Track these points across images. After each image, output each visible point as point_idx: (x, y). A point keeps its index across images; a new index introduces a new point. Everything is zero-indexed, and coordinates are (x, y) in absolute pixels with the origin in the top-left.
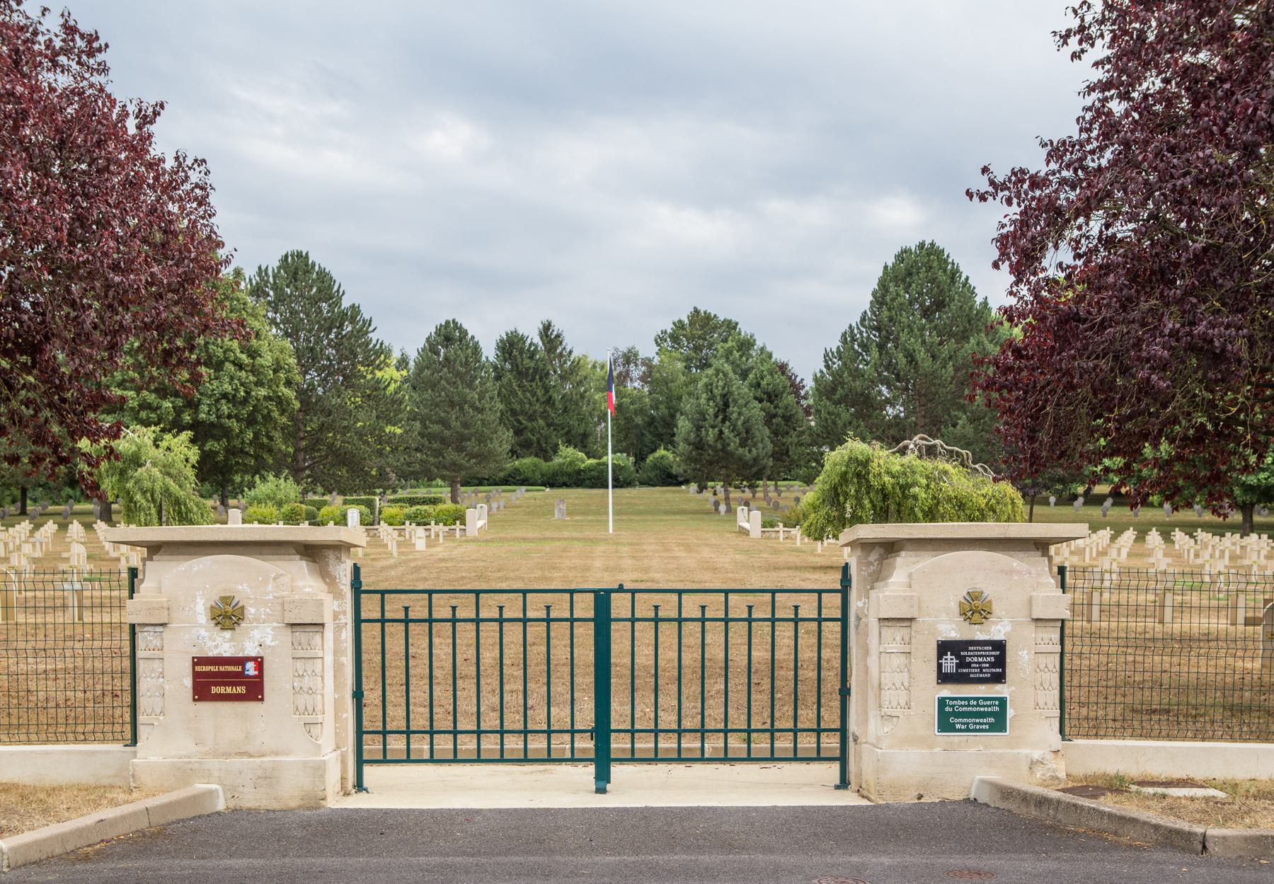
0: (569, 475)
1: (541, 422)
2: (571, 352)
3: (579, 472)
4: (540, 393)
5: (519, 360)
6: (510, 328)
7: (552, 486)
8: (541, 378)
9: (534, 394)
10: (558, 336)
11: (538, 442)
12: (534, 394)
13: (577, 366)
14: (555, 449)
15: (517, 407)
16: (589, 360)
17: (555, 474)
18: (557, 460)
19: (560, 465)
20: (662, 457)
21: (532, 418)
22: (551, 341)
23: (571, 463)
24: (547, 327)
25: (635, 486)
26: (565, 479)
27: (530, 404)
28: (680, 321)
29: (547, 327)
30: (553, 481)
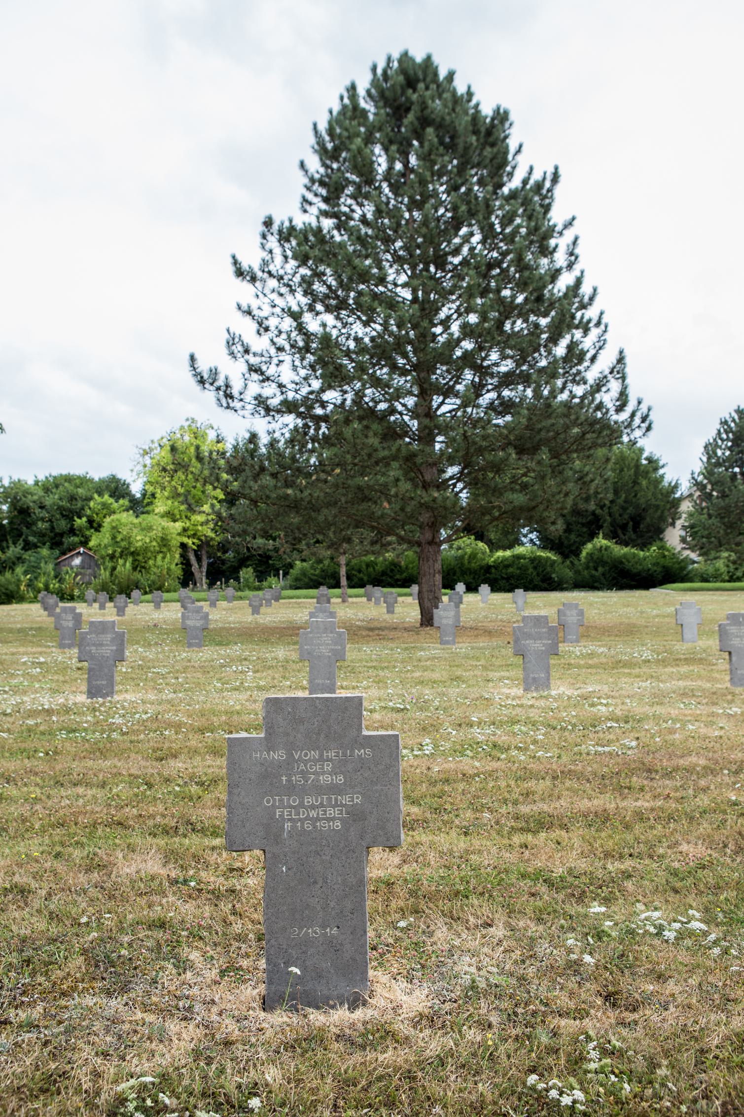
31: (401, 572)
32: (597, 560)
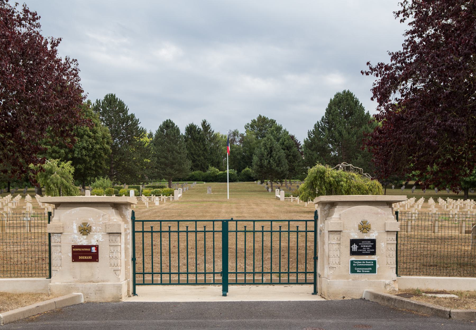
0: (213, 177)
1: (202, 158)
2: (213, 131)
3: (216, 176)
4: (202, 147)
5: (194, 134)
6: (191, 123)
7: (206, 181)
8: (202, 141)
9: (199, 147)
10: (208, 125)
11: (201, 165)
12: (199, 147)
13: (216, 136)
14: (207, 168)
15: (193, 152)
16: (220, 134)
17: (207, 177)
18: (208, 172)
19: (210, 174)
20: (248, 171)
21: (199, 156)
22: (206, 127)
23: (213, 173)
24: (204, 122)
25: (237, 181)
26: (211, 179)
27: (198, 151)
28: (254, 120)
29: (204, 122)
30: (207, 179)
31: (194, 177)
32: (245, 174)
